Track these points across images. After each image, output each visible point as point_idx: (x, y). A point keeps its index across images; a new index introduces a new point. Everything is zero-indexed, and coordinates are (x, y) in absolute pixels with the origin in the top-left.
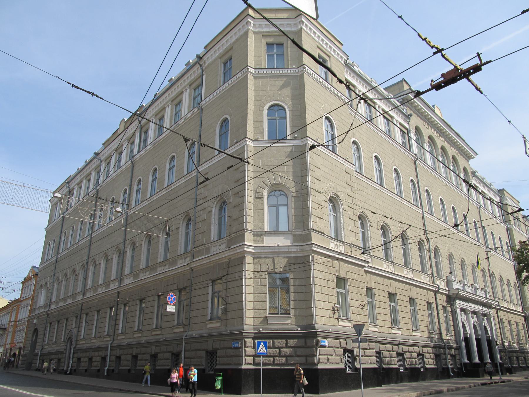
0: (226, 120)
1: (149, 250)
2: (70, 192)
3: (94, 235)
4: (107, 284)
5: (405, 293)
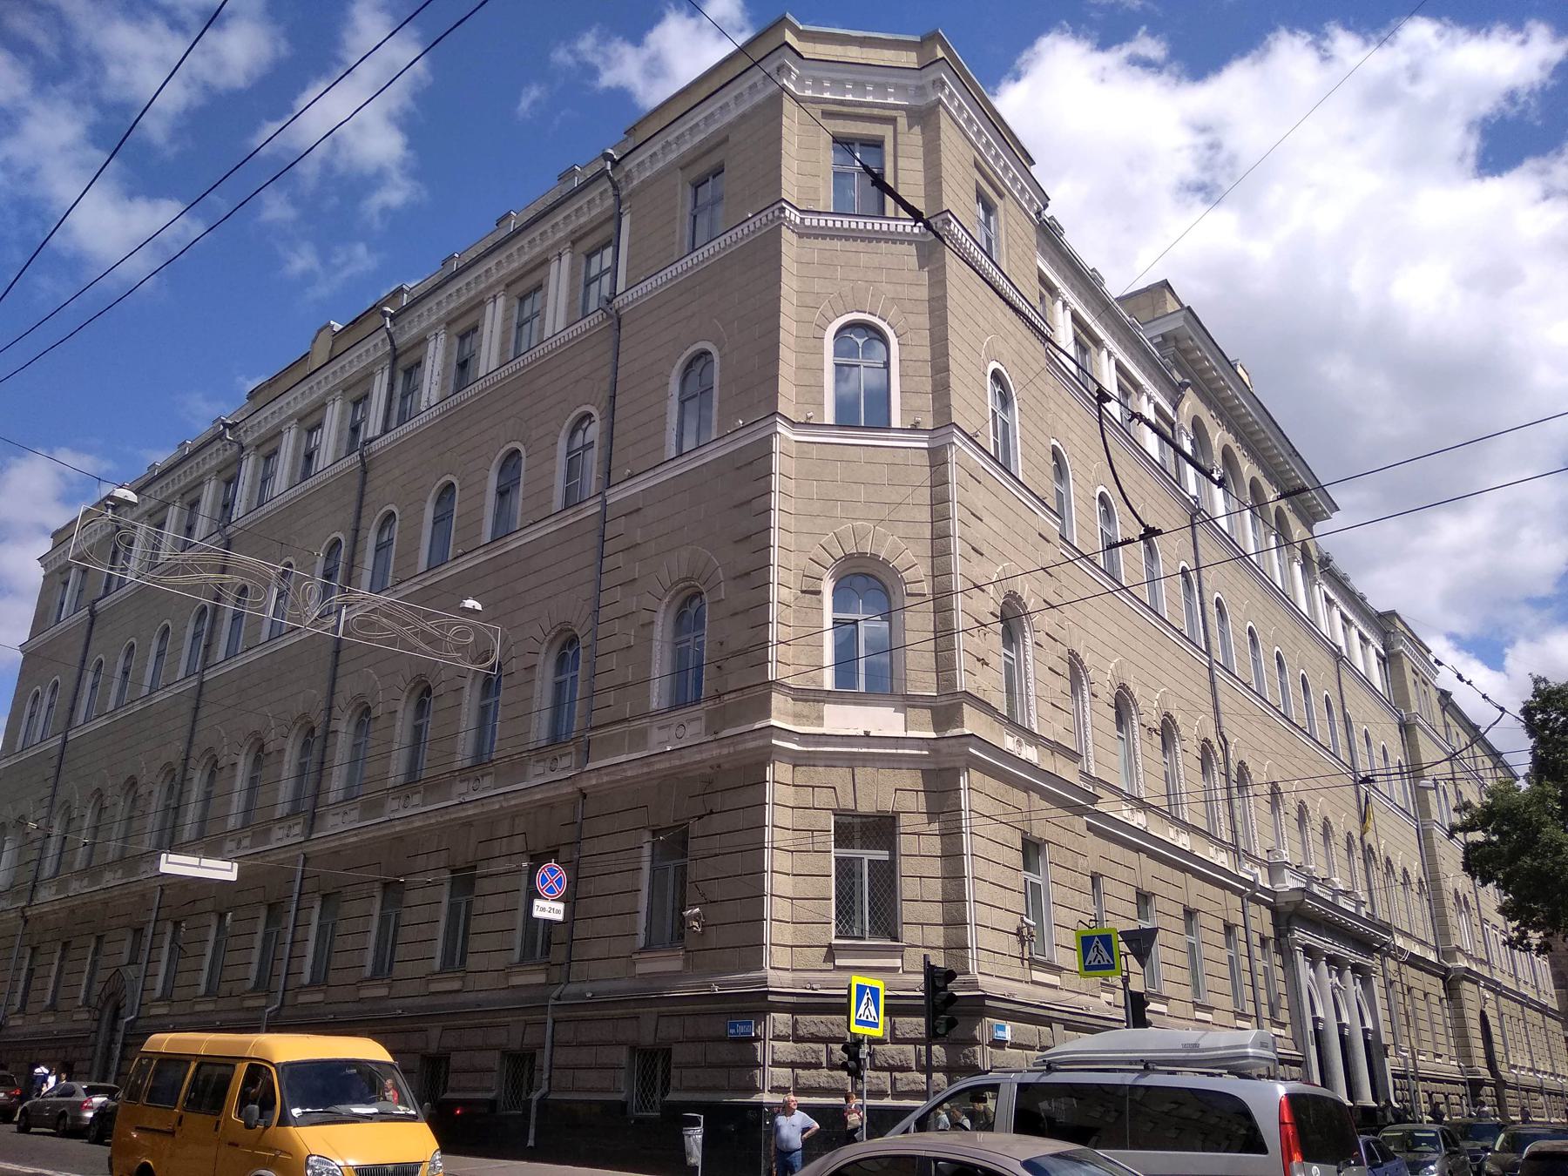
0: (450, 486)
1: (418, 731)
5: (1173, 893)
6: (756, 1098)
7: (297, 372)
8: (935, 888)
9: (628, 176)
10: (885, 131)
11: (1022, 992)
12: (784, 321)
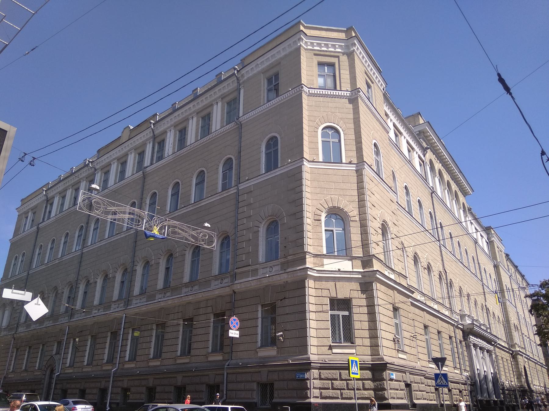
2: (47, 201)
3: (85, 250)
4: (105, 304)
6: (307, 401)
7: (116, 143)
8: (366, 325)
9: (243, 76)
10: (335, 60)
11: (396, 361)
12: (305, 126)
